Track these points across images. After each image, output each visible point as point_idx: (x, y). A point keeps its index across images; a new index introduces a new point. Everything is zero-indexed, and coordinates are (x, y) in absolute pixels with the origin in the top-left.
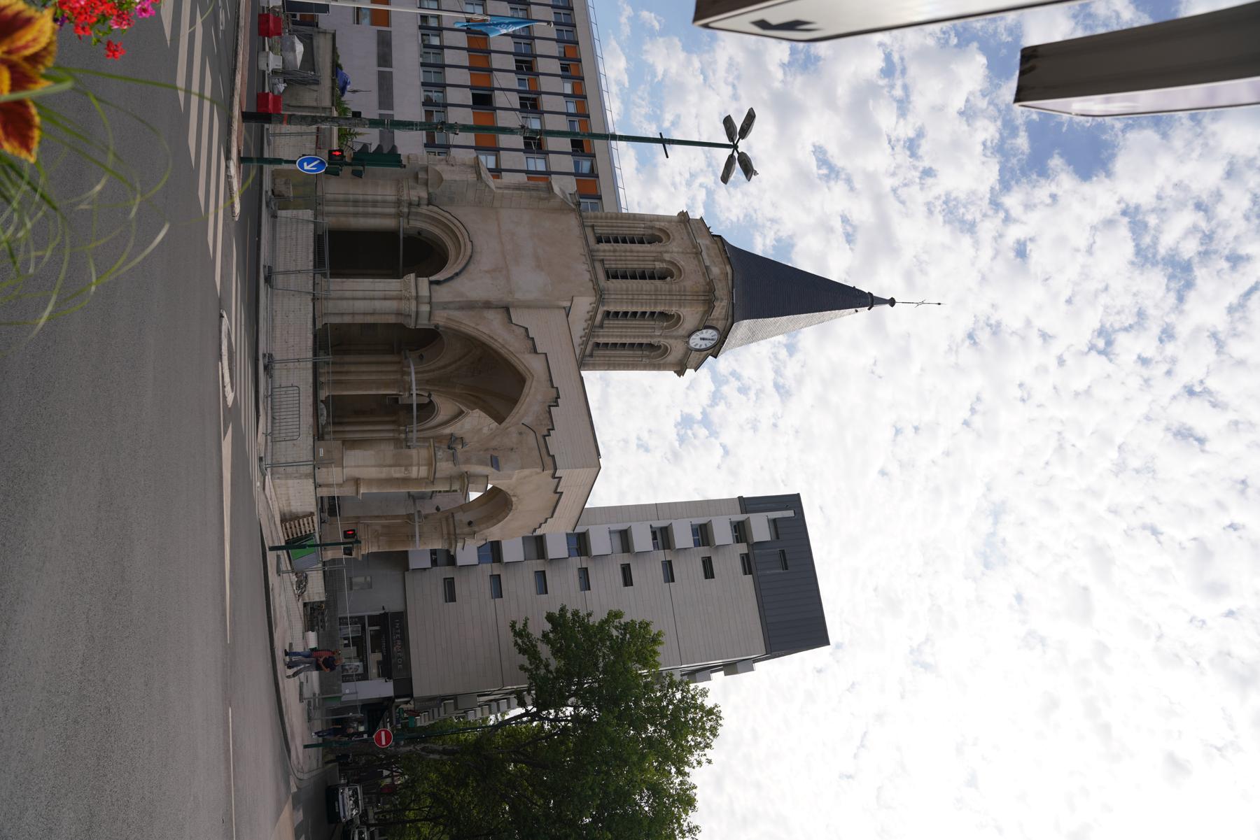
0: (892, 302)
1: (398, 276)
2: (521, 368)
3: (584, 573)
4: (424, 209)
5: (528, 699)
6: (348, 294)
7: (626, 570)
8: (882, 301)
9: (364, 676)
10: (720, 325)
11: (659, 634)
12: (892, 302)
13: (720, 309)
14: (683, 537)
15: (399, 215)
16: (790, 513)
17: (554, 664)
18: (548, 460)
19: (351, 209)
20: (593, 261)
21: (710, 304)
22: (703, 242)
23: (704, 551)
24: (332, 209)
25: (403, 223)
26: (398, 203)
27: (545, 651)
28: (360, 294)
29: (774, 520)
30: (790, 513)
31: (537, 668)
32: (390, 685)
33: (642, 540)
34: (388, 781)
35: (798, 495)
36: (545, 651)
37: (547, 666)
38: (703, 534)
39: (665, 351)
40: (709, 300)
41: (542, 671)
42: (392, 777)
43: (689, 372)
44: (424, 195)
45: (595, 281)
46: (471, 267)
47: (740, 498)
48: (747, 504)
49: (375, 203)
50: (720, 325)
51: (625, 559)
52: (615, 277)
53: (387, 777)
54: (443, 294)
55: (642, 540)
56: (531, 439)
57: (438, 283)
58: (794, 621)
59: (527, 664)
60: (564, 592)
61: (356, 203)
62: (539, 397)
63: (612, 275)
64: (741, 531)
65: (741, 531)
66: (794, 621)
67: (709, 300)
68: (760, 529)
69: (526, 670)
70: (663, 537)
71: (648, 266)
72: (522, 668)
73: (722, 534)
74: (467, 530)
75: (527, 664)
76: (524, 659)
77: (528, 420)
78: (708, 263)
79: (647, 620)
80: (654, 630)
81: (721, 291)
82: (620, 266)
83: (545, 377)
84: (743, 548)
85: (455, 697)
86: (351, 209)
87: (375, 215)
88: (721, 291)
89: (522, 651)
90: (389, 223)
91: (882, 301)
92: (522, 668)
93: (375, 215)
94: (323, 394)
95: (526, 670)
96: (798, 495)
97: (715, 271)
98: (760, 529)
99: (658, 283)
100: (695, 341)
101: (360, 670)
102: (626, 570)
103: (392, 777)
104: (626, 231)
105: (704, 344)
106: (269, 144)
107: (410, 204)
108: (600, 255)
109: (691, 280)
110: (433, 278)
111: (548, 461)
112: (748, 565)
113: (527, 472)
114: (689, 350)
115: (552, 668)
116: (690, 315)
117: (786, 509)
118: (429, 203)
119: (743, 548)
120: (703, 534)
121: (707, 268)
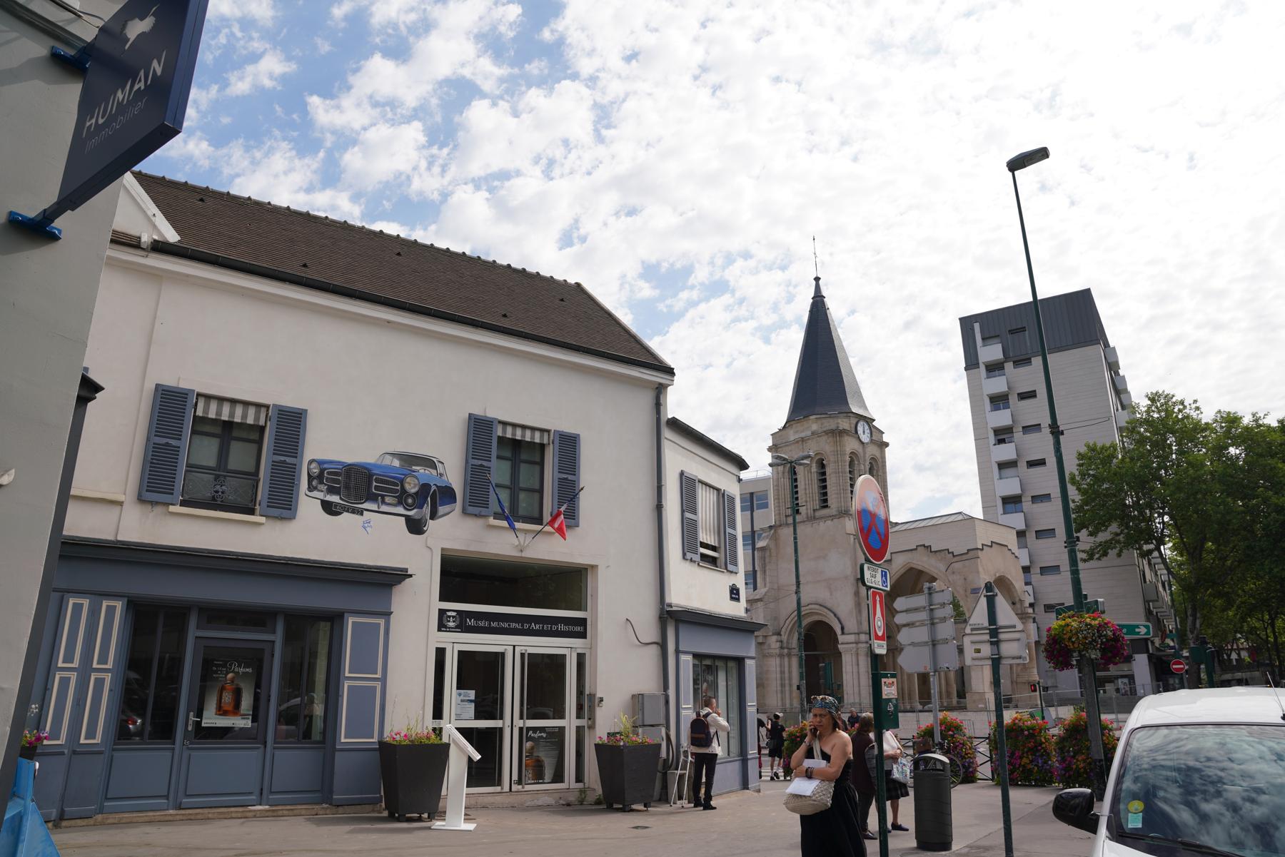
0: (817, 279)
1: (839, 655)
2: (903, 571)
3: (1035, 499)
4: (784, 638)
5: (1146, 547)
6: (856, 690)
7: (1032, 464)
8: (818, 288)
9: (1131, 678)
10: (854, 421)
11: (1088, 446)
12: (817, 279)
13: (844, 424)
14: (1002, 418)
15: (789, 655)
16: (977, 326)
17: (1114, 527)
18: (971, 554)
19: (787, 688)
20: (815, 518)
21: (841, 433)
22: (792, 436)
23: (1013, 399)
24: (788, 702)
25: (795, 651)
26: (781, 656)
27: (1103, 537)
28: (856, 682)
29: (983, 339)
30: (977, 326)
31: (1119, 542)
32: (1137, 656)
33: (1007, 452)
34: (1244, 654)
35: (961, 319)
36: (1103, 537)
37: (1117, 535)
38: (998, 401)
39: (873, 459)
40: (838, 433)
41: (1121, 538)
42: (1239, 650)
43: (885, 438)
44: (774, 638)
45: (832, 517)
46: (829, 605)
47: (966, 369)
48: (971, 362)
49: (782, 672)
50: (854, 421)
51: (1022, 464)
52: (826, 501)
53: (1239, 655)
54: (851, 625)
55: (1007, 452)
56: (956, 566)
57: (843, 628)
58: (1069, 322)
59: (1116, 551)
60: (1051, 516)
61: (783, 685)
62: (925, 559)
63: (824, 503)
64: (994, 368)
65: (994, 368)
66: (1069, 322)
67: (838, 433)
68: (992, 352)
69: (1121, 551)
70: (1002, 435)
71: (815, 477)
72: (1119, 555)
73: (998, 385)
74: (1018, 606)
75: (1116, 551)
76: (1112, 553)
77: (942, 567)
78: (809, 433)
79: (1076, 455)
80: (1083, 450)
81: (830, 424)
82: (817, 497)
83: (909, 554)
84: (1009, 366)
85: (1146, 602)
86: (787, 688)
87: (790, 672)
88: (830, 424)
89: (1105, 554)
90: (795, 661)
91: (818, 288)
92: (1119, 555)
93: (790, 672)
94: (920, 707)
95: (1121, 551)
96: (961, 319)
97: (815, 427)
98: (992, 352)
99: (828, 470)
100: (865, 438)
101: (1126, 680)
102: (1032, 464)
103: (1239, 650)
104: (788, 492)
105: (867, 431)
106: (351, 832)
107: (782, 648)
108: (810, 512)
109: (825, 446)
110: (838, 631)
111: (971, 554)
112: (1022, 361)
113: (981, 569)
114: (872, 441)
115: (1119, 531)
116: (850, 445)
117: (973, 329)
118: (779, 634)
119: (1009, 366)
120: (998, 401)
121: (813, 433)
